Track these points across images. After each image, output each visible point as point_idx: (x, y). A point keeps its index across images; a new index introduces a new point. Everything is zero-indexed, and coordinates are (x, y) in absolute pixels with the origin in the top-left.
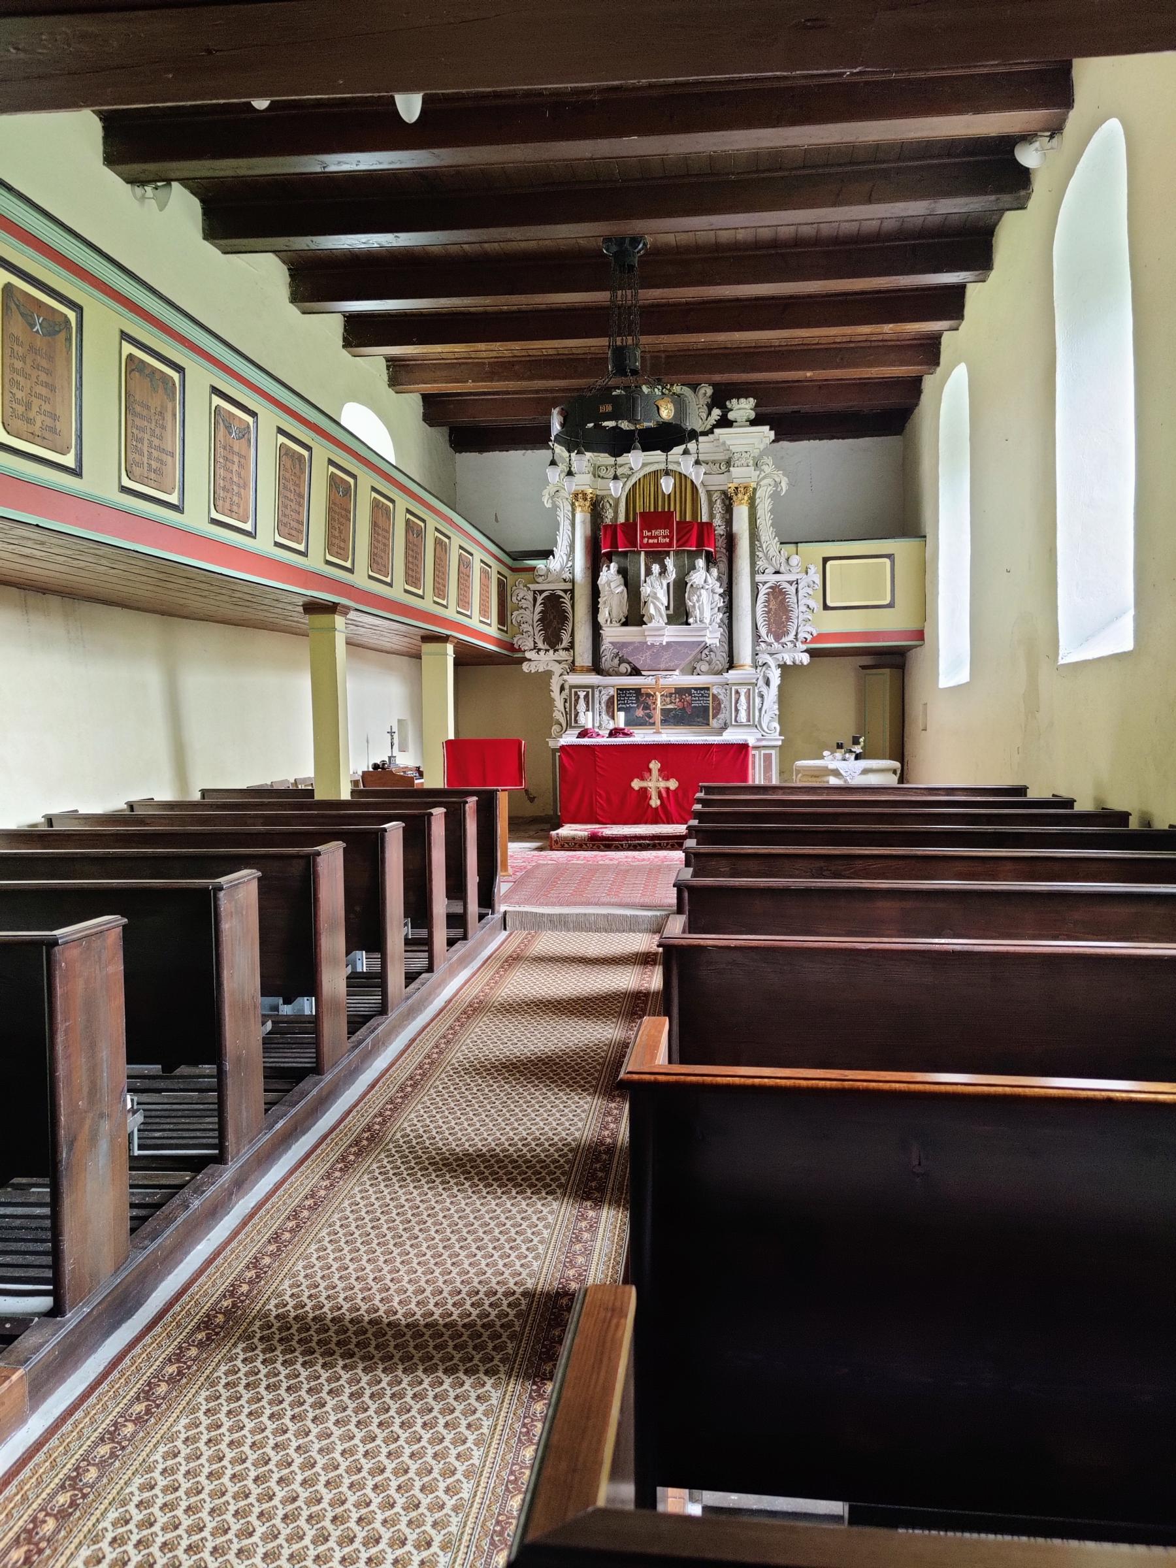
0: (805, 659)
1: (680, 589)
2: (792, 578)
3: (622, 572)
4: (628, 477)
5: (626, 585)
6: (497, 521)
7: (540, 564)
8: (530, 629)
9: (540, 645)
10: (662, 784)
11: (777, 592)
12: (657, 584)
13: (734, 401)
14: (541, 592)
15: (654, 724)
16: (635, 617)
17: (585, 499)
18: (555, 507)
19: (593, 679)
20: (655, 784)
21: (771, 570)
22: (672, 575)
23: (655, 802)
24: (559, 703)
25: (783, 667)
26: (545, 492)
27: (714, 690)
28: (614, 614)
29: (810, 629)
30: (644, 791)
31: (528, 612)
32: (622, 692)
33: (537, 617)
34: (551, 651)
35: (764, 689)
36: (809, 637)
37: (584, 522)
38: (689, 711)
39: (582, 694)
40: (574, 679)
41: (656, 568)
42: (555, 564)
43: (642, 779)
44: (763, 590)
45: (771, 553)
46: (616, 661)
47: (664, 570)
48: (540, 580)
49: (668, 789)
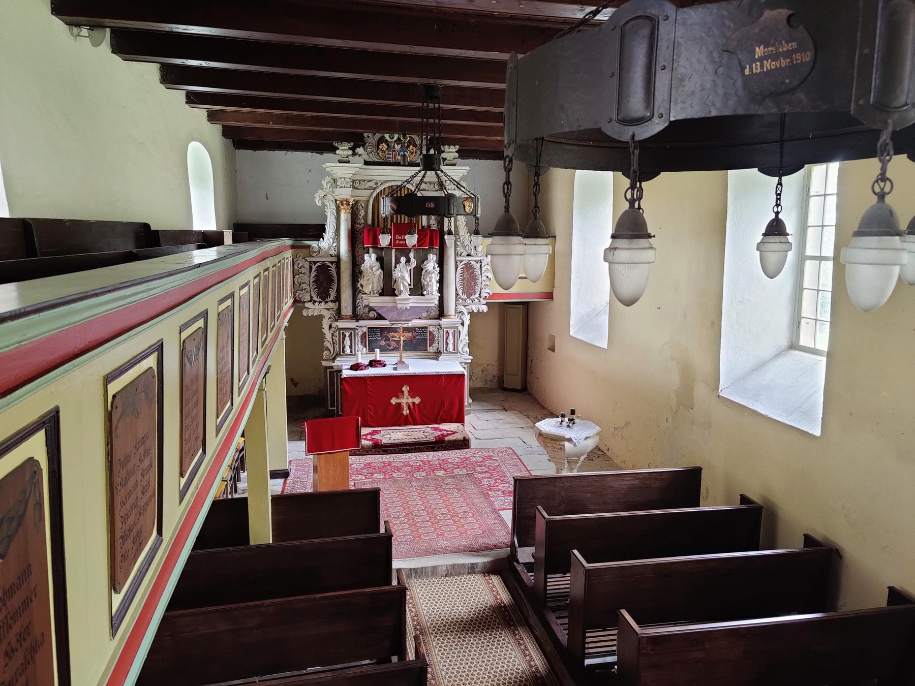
0: (485, 309)
1: (418, 273)
2: (478, 259)
3: (380, 259)
4: (374, 189)
5: (382, 268)
6: (267, 198)
7: (314, 244)
8: (308, 287)
9: (315, 298)
10: (410, 401)
11: (468, 267)
12: (404, 270)
13: (446, 147)
14: (315, 263)
15: (396, 349)
16: (388, 289)
17: (348, 205)
18: (324, 205)
19: (353, 324)
20: (406, 400)
21: (465, 253)
22: (414, 263)
23: (406, 412)
24: (328, 336)
25: (471, 313)
26: (317, 195)
27: (431, 329)
28: (375, 289)
29: (488, 291)
30: (399, 405)
31: (306, 276)
32: (371, 330)
33: (312, 281)
34: (323, 303)
35: (460, 327)
36: (488, 296)
37: (347, 220)
38: (414, 341)
39: (347, 334)
40: (341, 324)
41: (403, 260)
42: (326, 243)
43: (398, 397)
44: (460, 266)
45: (466, 243)
46: (367, 309)
47: (408, 261)
48: (314, 255)
49: (414, 403)
